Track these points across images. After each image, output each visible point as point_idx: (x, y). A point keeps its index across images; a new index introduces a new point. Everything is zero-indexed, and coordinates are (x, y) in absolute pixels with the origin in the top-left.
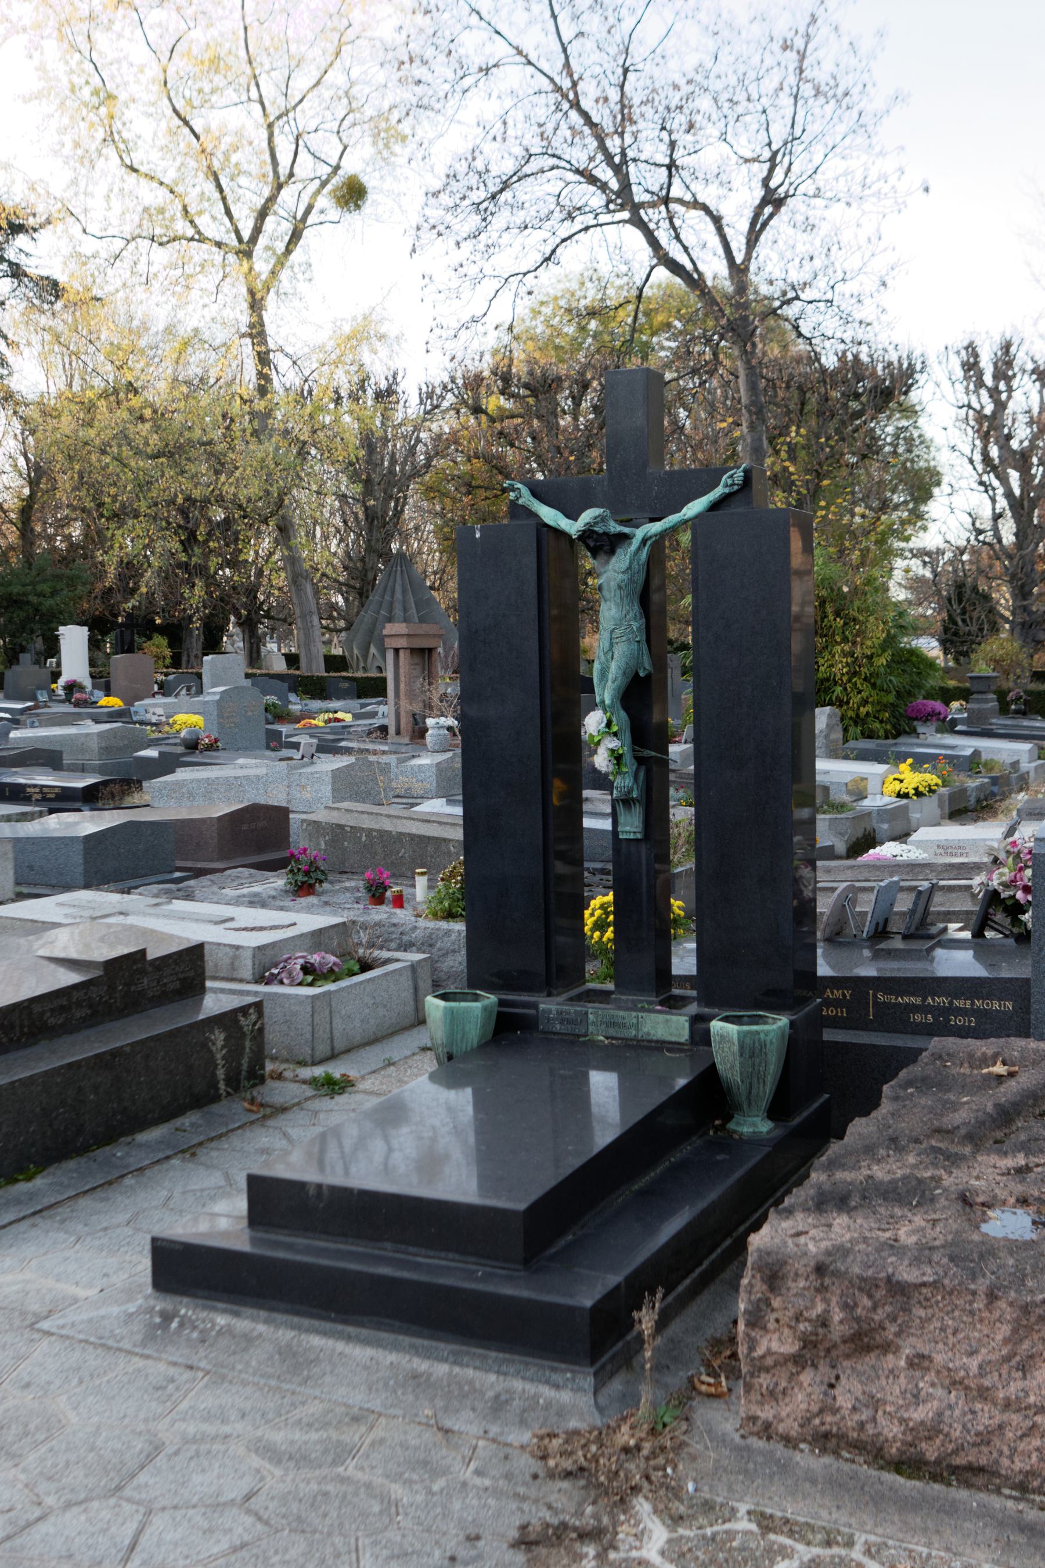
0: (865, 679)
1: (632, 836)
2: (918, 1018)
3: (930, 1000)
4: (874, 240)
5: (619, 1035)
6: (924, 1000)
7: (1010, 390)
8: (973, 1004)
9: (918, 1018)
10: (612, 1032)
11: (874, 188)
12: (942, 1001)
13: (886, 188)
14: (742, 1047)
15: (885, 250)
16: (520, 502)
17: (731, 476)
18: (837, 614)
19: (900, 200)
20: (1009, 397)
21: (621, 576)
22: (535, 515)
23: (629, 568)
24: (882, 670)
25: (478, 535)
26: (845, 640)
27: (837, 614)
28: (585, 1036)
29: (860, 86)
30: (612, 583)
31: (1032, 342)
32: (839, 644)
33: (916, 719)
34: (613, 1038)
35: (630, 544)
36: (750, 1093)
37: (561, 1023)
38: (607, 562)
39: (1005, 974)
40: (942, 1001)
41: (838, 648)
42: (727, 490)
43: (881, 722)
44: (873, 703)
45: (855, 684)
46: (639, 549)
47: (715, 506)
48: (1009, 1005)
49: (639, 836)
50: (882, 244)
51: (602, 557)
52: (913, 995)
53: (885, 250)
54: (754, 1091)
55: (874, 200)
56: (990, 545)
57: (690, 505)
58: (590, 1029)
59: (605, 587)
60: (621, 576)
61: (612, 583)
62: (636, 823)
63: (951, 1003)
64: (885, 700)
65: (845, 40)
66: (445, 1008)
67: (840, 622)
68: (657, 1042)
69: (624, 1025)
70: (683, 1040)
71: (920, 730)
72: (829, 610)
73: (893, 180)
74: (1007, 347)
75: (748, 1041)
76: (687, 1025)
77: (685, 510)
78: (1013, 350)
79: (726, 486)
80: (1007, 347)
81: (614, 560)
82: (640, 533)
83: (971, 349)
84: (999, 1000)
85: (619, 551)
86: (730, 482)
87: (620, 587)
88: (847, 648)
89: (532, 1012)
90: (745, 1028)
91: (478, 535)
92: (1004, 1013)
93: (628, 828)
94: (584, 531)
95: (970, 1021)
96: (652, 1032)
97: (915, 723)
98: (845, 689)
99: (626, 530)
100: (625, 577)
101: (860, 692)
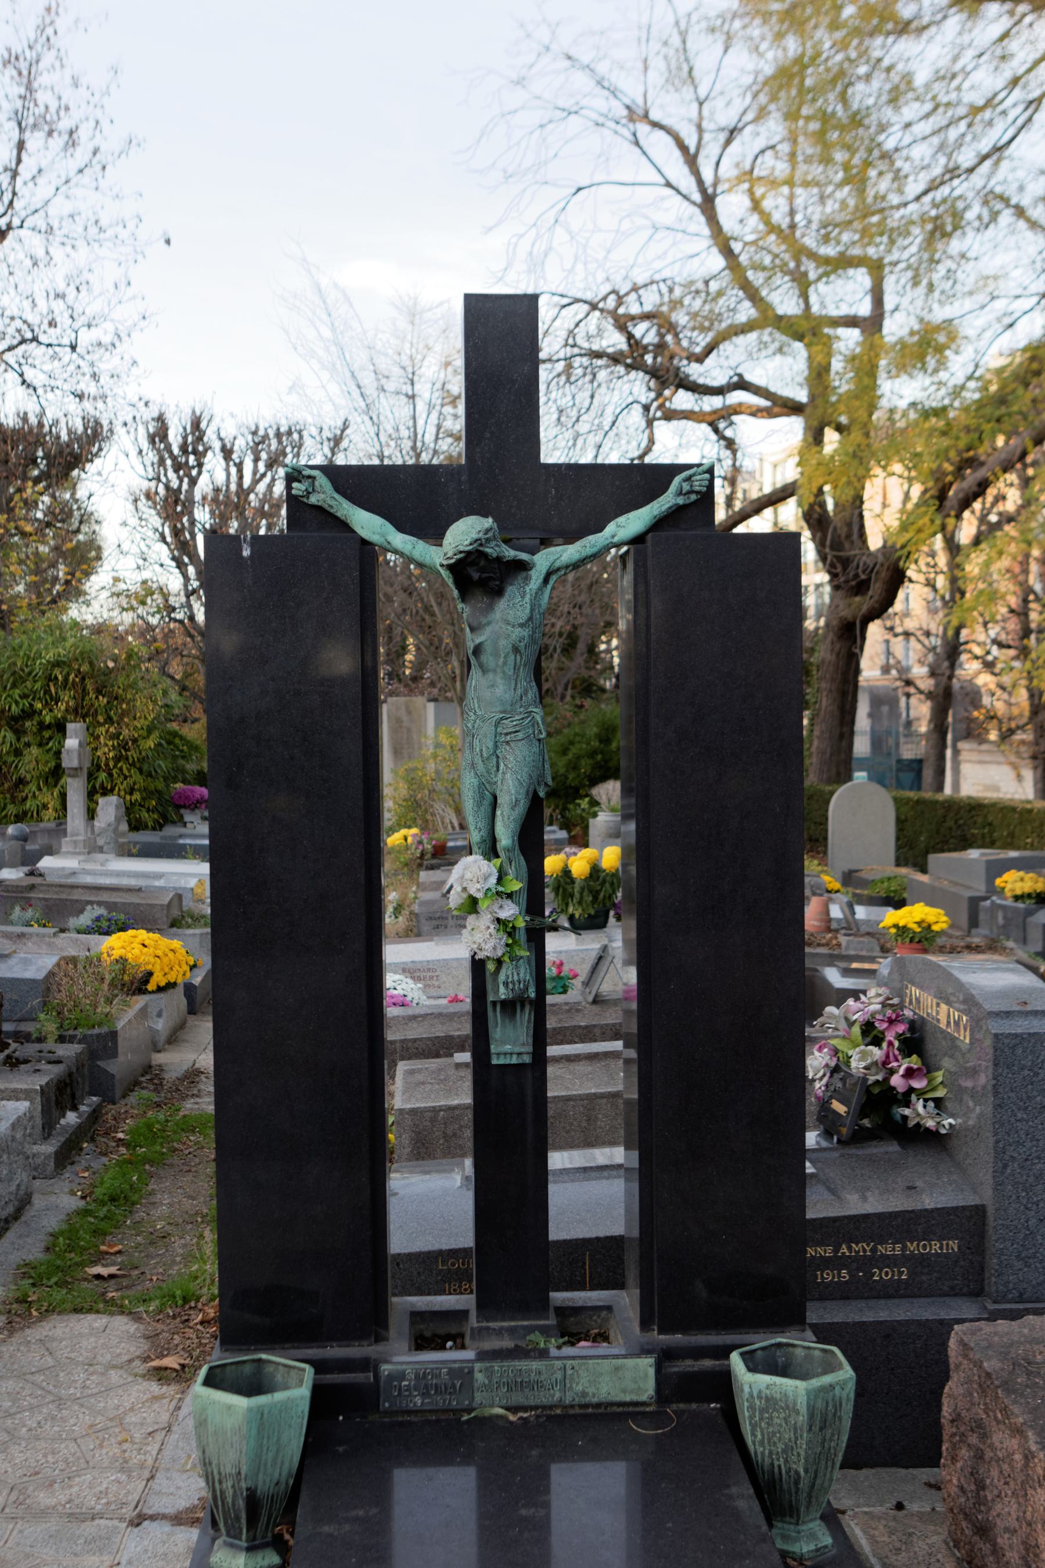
0: (133, 765)
1: (514, 1060)
2: (828, 1276)
3: (844, 1249)
4: (122, 286)
5: (532, 1402)
6: (836, 1250)
7: (200, 465)
8: (904, 1248)
9: (828, 1276)
10: (517, 1398)
11: (110, 233)
12: (862, 1248)
13: (124, 234)
14: (811, 1416)
15: (134, 298)
16: (313, 500)
17: (688, 479)
18: (99, 692)
19: (139, 249)
20: (200, 473)
21: (518, 632)
22: (344, 526)
23: (530, 619)
24: (150, 754)
25: (246, 553)
26: (109, 720)
27: (99, 692)
28: (469, 1411)
29: (92, 124)
30: (503, 643)
31: (223, 420)
32: (103, 725)
33: (185, 807)
34: (525, 1409)
35: (527, 579)
36: (813, 1485)
37: (425, 1395)
38: (490, 608)
39: (929, 1201)
40: (862, 1248)
41: (103, 729)
42: (681, 501)
43: (148, 811)
44: (139, 790)
45: (121, 769)
46: (541, 589)
47: (658, 525)
48: (954, 1245)
49: (527, 1059)
50: (130, 292)
51: (481, 600)
52: (821, 1244)
53: (134, 298)
54: (818, 1481)
55: (110, 244)
56: (181, 622)
57: (621, 520)
58: (479, 1397)
59: (488, 648)
60: (518, 632)
61: (503, 643)
62: (523, 1038)
63: (874, 1250)
64: (152, 787)
65: (68, 72)
66: (250, 1410)
67: (102, 700)
68: (598, 1405)
69: (539, 1385)
70: (644, 1398)
71: (188, 818)
72: (90, 686)
73: (131, 225)
74: (196, 423)
75: (820, 1404)
76: (652, 1371)
77: (610, 528)
78: (203, 425)
79: (680, 493)
80: (196, 423)
81: (502, 604)
82: (543, 560)
83: (161, 419)
84: (941, 1239)
85: (511, 590)
86: (686, 487)
87: (516, 650)
88: (112, 730)
89: (358, 1377)
90: (816, 1383)
91: (246, 553)
92: (947, 1256)
93: (508, 1048)
94: (469, 553)
95: (901, 1273)
96: (591, 1390)
97: (182, 811)
98: (111, 775)
99: (524, 556)
100: (525, 633)
101: (126, 778)
